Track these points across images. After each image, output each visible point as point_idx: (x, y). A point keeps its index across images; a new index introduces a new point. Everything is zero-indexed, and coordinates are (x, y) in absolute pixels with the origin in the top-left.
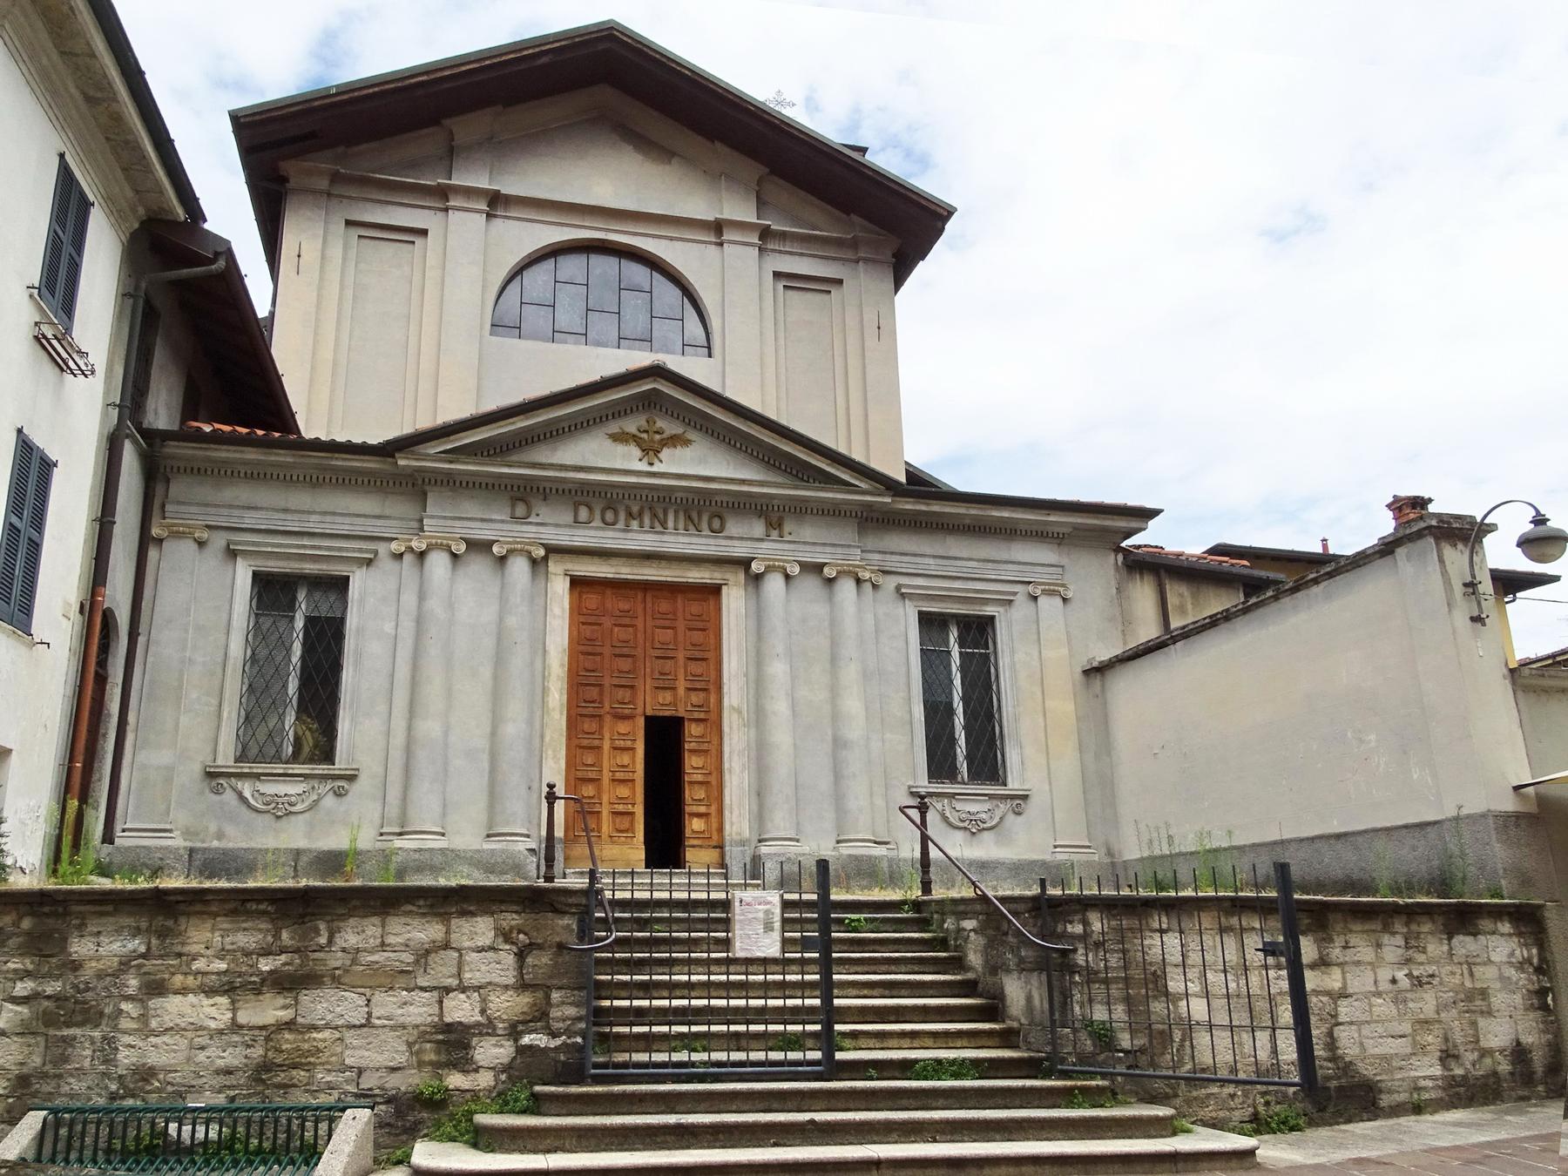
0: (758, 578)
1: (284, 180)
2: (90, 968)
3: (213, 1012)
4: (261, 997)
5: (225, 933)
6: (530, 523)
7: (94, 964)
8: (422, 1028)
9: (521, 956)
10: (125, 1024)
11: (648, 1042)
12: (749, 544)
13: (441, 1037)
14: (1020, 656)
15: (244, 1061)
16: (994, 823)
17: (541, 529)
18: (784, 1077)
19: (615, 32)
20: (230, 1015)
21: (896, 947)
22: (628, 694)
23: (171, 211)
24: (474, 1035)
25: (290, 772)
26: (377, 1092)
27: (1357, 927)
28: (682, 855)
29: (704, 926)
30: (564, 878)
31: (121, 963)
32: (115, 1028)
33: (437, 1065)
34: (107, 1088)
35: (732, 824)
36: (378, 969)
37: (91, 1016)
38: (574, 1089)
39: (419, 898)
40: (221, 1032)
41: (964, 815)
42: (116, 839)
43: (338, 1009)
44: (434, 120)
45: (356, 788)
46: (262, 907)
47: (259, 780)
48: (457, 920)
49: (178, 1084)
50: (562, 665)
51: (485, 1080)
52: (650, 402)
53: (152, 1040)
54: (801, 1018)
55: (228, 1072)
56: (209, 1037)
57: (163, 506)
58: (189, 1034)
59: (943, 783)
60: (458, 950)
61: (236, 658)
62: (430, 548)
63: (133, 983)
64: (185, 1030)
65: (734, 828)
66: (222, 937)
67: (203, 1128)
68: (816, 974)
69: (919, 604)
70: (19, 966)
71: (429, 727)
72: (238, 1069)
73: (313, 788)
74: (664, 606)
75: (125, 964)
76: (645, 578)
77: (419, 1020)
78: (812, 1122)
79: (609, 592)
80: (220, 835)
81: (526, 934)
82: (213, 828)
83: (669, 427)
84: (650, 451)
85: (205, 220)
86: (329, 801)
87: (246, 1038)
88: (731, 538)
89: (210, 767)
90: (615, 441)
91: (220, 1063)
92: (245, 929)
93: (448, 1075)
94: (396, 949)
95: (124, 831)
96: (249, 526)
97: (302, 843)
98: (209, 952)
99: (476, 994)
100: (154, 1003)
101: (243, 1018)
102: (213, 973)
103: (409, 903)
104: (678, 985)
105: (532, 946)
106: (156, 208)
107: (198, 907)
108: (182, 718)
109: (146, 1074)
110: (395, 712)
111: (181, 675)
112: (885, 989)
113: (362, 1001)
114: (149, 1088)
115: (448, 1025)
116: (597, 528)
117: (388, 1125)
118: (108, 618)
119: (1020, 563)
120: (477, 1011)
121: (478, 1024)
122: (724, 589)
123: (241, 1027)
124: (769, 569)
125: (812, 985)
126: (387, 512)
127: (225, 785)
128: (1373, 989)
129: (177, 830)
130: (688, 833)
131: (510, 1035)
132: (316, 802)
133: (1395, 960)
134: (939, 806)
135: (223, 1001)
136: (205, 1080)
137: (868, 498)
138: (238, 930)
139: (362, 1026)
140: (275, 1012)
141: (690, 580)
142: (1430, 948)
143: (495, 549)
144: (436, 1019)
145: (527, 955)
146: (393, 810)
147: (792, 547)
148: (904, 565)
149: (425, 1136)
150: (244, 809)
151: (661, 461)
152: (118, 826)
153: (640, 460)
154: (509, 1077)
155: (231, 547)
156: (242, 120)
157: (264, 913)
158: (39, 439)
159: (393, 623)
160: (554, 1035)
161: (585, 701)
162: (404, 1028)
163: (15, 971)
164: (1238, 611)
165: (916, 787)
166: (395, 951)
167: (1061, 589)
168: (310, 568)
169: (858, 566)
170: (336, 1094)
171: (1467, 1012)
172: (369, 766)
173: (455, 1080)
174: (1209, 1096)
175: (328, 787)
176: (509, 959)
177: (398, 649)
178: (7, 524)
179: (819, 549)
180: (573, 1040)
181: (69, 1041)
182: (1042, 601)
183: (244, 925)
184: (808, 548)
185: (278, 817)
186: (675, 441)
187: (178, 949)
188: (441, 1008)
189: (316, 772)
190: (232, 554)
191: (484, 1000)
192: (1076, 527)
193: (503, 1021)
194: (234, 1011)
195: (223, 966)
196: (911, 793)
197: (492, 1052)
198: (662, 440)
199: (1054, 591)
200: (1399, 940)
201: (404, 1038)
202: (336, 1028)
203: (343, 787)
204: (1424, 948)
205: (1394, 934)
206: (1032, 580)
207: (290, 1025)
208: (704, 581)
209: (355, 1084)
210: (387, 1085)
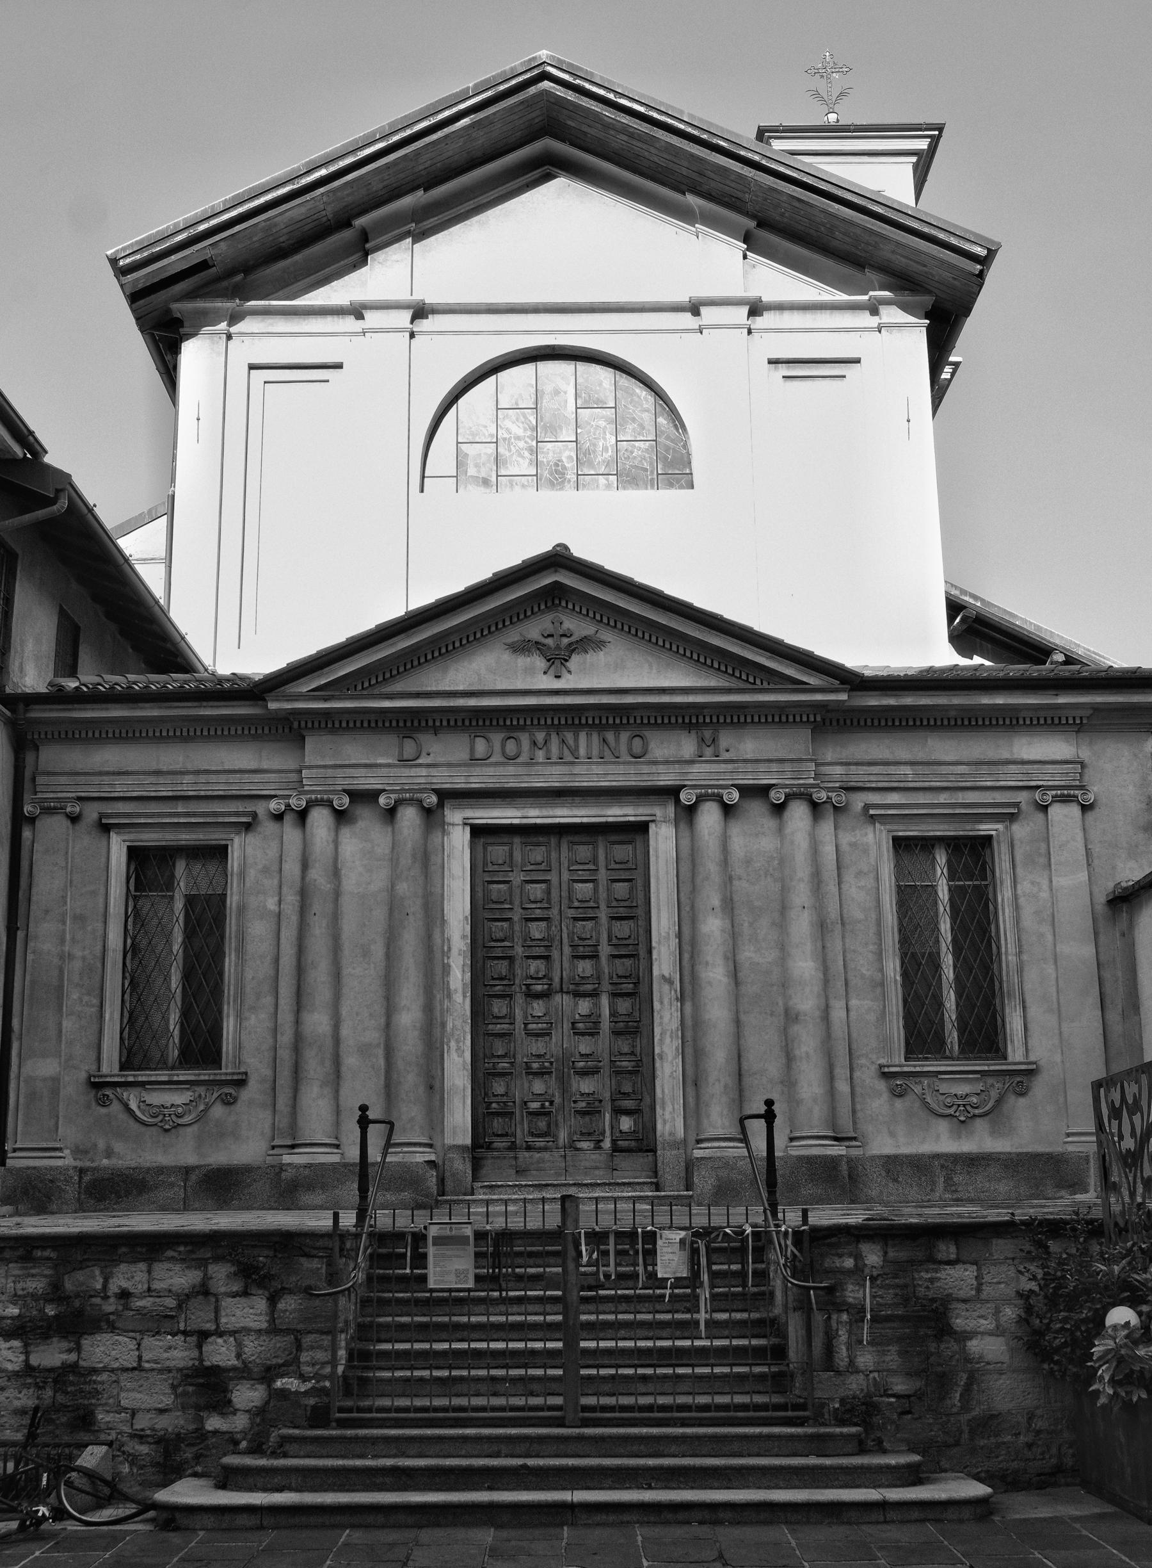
0: (691, 811)
3: (9, 1355)
5: (17, 1279)
6: (420, 765)
8: (185, 1372)
9: (273, 1300)
12: (677, 768)
13: (201, 1381)
14: (1024, 887)
16: (987, 1108)
20: (22, 1357)
23: (9, 450)
24: (231, 1379)
25: (175, 1078)
26: (148, 1432)
30: (472, 1194)
35: (665, 1122)
36: (145, 1315)
39: (179, 1244)
40: (16, 1374)
41: (949, 1100)
42: (8, 1161)
43: (114, 1353)
45: (245, 1094)
46: (47, 1253)
47: (146, 1089)
48: (213, 1266)
50: (464, 937)
51: (240, 1422)
52: (555, 596)
56: (6, 1378)
57: (34, 780)
59: (926, 1059)
60: (215, 1295)
61: (114, 951)
62: (311, 804)
65: (667, 1127)
66: (14, 1282)
68: (559, 1314)
69: (895, 827)
71: (318, 1022)
73: (200, 1096)
74: (583, 852)
76: (557, 820)
77: (181, 1364)
78: (525, 1466)
79: (517, 840)
80: (109, 1153)
82: (101, 1145)
83: (577, 626)
84: (557, 659)
86: (218, 1111)
87: (38, 1380)
88: (655, 763)
89: (95, 1076)
90: (515, 651)
92: (33, 1276)
93: (208, 1417)
94: (161, 1294)
95: (15, 1150)
96: (121, 794)
97: (191, 1159)
99: (232, 1339)
101: (34, 1361)
102: (8, 1318)
103: (171, 1248)
108: (65, 1023)
110: (282, 1002)
111: (61, 971)
113: (132, 1345)
115: (207, 1368)
116: (496, 764)
117: (158, 1463)
119: (1023, 762)
120: (233, 1355)
121: (234, 1369)
122: (652, 827)
124: (701, 799)
126: (265, 765)
127: (111, 1096)
132: (206, 1110)
134: (917, 1089)
135: (16, 1343)
136: (5, 1419)
137: (819, 697)
139: (134, 1369)
140: (61, 1356)
141: (610, 819)
143: (382, 800)
144: (197, 1363)
146: (283, 1122)
147: (730, 767)
148: (872, 778)
149: (195, 1475)
150: (132, 1122)
151: (569, 672)
153: (545, 673)
155: (104, 821)
156: (121, 263)
159: (276, 899)
160: (303, 1378)
162: (170, 1371)
165: (888, 1066)
166: (160, 1297)
168: (185, 838)
169: (813, 786)
172: (257, 1066)
173: (214, 1423)
174: (998, 1445)
175: (216, 1095)
177: (283, 929)
179: (762, 767)
180: (322, 1384)
182: (1056, 811)
183: (33, 1271)
184: (750, 767)
185: (167, 1131)
186: (585, 644)
188: (201, 1353)
189: (202, 1078)
190: (105, 829)
191: (239, 1345)
192: (1096, 709)
194: (27, 1354)
196: (884, 1073)
197: (247, 1396)
198: (570, 644)
199: (1069, 796)
201: (170, 1382)
202: (113, 1371)
203: (231, 1094)
206: (1041, 783)
208: (627, 819)
209: (129, 1424)
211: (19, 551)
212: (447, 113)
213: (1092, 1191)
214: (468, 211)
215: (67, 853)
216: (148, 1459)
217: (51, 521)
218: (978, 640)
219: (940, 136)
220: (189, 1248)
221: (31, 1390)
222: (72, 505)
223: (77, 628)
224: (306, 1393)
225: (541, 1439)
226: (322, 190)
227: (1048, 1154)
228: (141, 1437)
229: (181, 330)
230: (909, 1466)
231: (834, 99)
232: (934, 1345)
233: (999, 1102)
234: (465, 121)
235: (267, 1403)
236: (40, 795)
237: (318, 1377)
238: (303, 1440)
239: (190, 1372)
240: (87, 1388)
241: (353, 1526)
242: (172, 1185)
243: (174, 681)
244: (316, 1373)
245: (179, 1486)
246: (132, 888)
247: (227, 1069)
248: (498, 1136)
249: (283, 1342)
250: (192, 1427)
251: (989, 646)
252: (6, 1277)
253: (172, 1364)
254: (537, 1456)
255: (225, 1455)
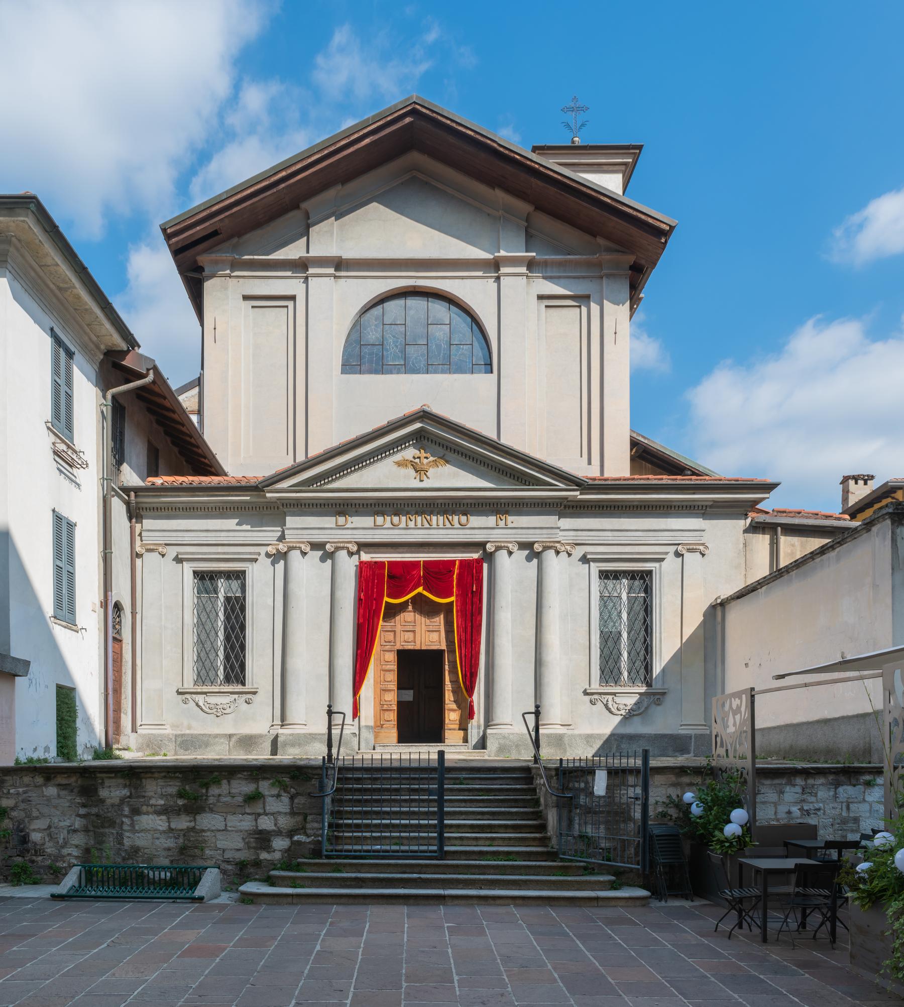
1: (201, 269)
2: (109, 802)
3: (160, 822)
4: (180, 816)
6: (348, 529)
7: (109, 800)
8: (249, 832)
9: (292, 798)
10: (125, 827)
11: (358, 840)
15: (175, 845)
16: (640, 711)
17: (355, 532)
18: (396, 858)
19: (418, 107)
20: (167, 824)
21: (507, 793)
22: (411, 635)
24: (272, 835)
26: (231, 860)
27: (768, 782)
28: (443, 735)
29: (408, 782)
31: (120, 800)
32: (122, 829)
33: (254, 848)
34: (121, 855)
37: (112, 823)
38: (317, 861)
39: (244, 771)
40: (164, 832)
43: (212, 822)
44: (295, 206)
45: (256, 699)
49: (149, 854)
53: (137, 834)
54: (407, 830)
55: (169, 849)
57: (140, 535)
58: (152, 832)
63: (126, 810)
64: (149, 830)
67: (164, 873)
70: (80, 801)
72: (173, 848)
75: (122, 800)
77: (247, 828)
78: (420, 878)
81: (294, 788)
85: (139, 346)
91: (166, 845)
92: (170, 786)
95: (141, 725)
98: (156, 796)
100: (136, 818)
101: (173, 826)
104: (414, 813)
105: (298, 794)
106: (110, 344)
107: (149, 775)
109: (136, 850)
112: (490, 815)
113: (222, 819)
114: (138, 855)
115: (260, 830)
117: (237, 874)
118: (118, 607)
120: (273, 824)
121: (274, 831)
123: (173, 830)
125: (434, 813)
127: (190, 699)
128: (773, 817)
129: (167, 724)
130: (447, 721)
131: (288, 836)
133: (793, 800)
135: (164, 817)
136: (160, 853)
138: (168, 785)
139: (223, 830)
142: (820, 794)
144: (255, 828)
145: (296, 798)
149: (256, 880)
152: (139, 723)
154: (289, 855)
155: (180, 556)
157: (178, 778)
158: (64, 512)
160: (308, 836)
161: (385, 642)
162: (241, 831)
163: (79, 803)
164: (793, 567)
167: (701, 548)
170: (214, 860)
171: (841, 830)
173: (264, 856)
176: (285, 799)
178: (55, 565)
180: (317, 838)
181: (103, 835)
183: (171, 783)
185: (217, 716)
187: (144, 794)
191: (276, 820)
193: (285, 829)
194: (169, 822)
195: (162, 802)
197: (280, 844)
200: (798, 789)
202: (212, 831)
204: (816, 793)
205: (794, 785)
206: (680, 542)
207: (193, 829)
210: (236, 857)
211: (126, 405)
212: (356, 136)
213: (692, 752)
214: (356, 206)
215: (161, 573)
216: (232, 872)
217: (142, 388)
218: (644, 462)
219: (640, 153)
220: (249, 773)
221: (172, 840)
222: (104, 391)
223: (157, 450)
224: (309, 843)
225: (427, 866)
226: (283, 185)
227: (671, 735)
228: (228, 862)
229: (203, 273)
230: (609, 881)
231: (578, 128)
232: (7, 821)
233: (647, 708)
234: (367, 141)
235: (290, 847)
236: (144, 542)
237: (316, 835)
238: (310, 864)
239: (251, 832)
240: (200, 839)
241: (337, 904)
242: (222, 743)
243: (215, 480)
244: (315, 834)
245: (248, 884)
246: (196, 592)
247: (248, 687)
248: (388, 721)
249: (299, 818)
250: (253, 858)
251: (650, 466)
252: (157, 786)
253: (242, 828)
254: (425, 873)
255: (270, 871)
